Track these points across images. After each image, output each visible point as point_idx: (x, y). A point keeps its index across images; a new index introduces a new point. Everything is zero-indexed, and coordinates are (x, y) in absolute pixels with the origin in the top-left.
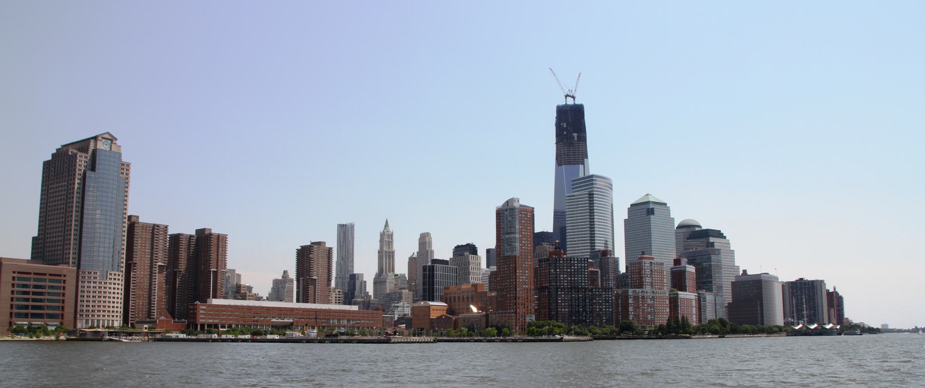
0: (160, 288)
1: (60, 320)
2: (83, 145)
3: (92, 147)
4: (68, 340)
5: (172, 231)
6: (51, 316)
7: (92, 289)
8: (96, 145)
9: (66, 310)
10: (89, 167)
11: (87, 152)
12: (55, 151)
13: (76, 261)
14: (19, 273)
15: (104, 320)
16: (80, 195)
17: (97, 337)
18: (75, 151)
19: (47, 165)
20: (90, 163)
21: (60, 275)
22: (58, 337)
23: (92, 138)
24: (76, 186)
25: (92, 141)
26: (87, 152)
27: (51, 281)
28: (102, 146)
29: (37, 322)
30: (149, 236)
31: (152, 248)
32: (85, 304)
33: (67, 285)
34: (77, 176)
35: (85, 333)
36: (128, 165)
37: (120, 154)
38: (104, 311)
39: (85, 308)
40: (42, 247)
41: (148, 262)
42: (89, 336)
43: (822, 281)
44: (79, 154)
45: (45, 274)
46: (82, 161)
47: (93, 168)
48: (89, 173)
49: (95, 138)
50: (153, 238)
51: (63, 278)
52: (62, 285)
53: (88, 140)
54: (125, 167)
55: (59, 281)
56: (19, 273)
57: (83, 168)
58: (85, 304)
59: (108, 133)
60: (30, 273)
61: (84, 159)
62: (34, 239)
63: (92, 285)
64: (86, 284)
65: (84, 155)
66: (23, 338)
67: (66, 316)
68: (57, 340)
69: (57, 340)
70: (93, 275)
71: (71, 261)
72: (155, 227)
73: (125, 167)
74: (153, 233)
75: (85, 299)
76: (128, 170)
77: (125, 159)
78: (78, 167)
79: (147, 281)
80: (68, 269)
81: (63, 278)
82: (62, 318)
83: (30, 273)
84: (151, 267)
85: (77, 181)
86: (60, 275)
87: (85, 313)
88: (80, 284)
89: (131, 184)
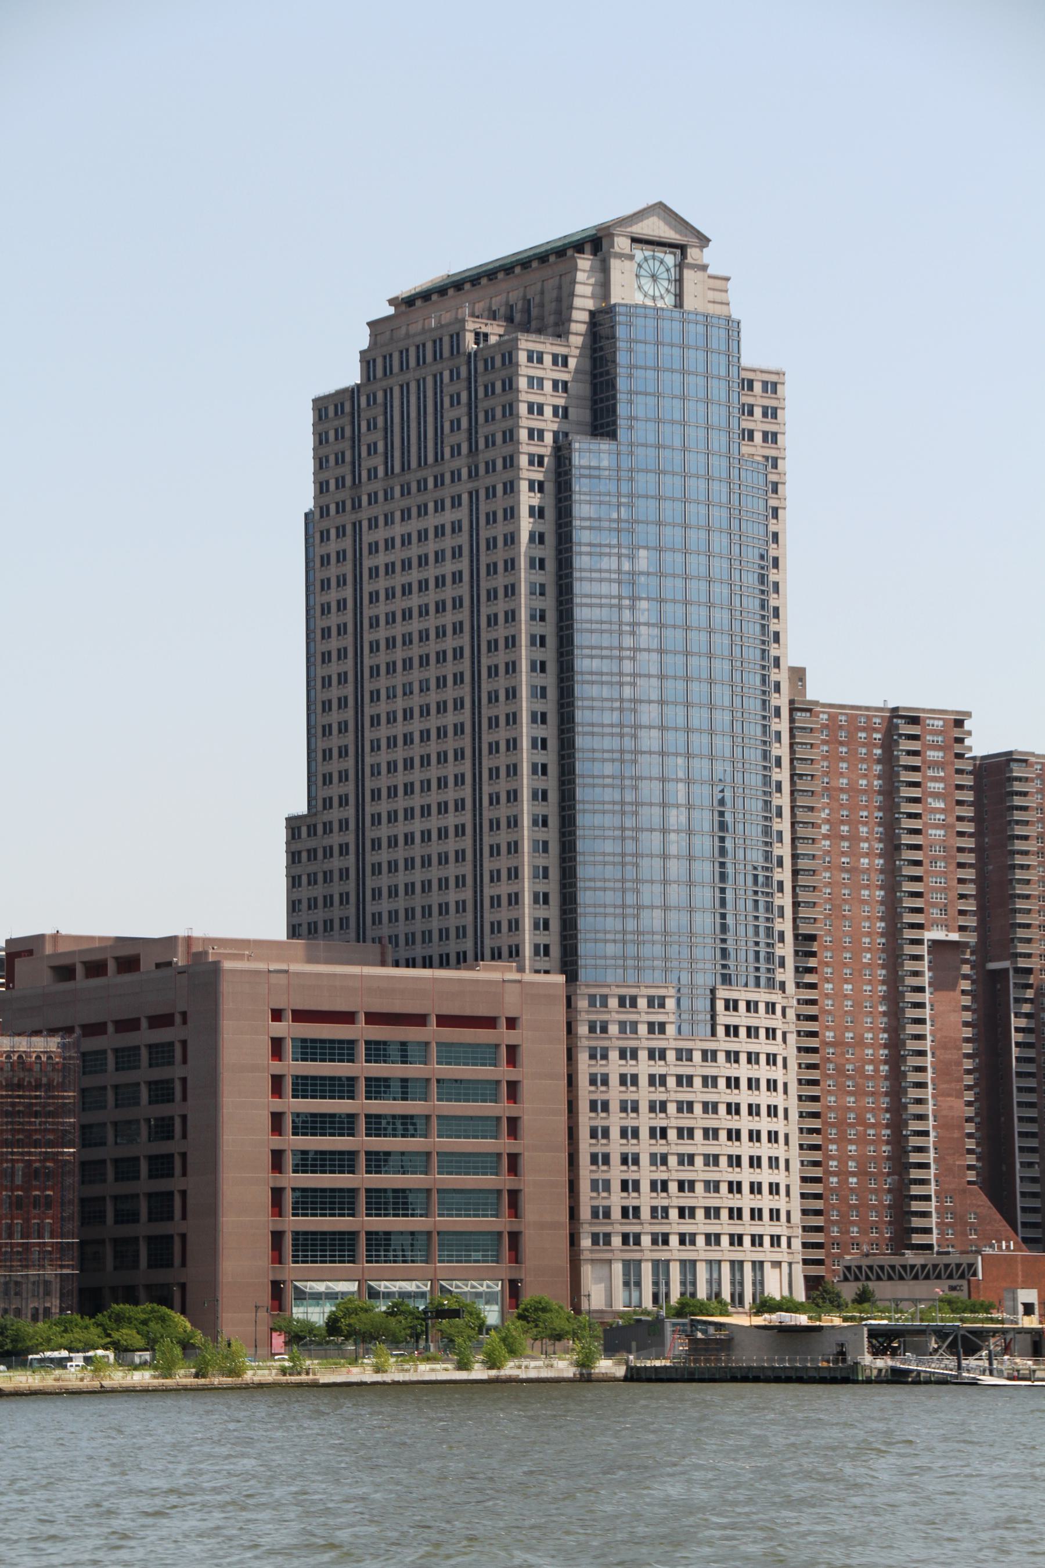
0: (943, 1071)
1: (505, 1269)
2: (532, 284)
3: (584, 300)
4: (634, 1376)
5: (982, 743)
6: (460, 1245)
7: (644, 1094)
8: (604, 286)
9: (530, 1210)
10: (580, 414)
11: (560, 330)
12: (363, 340)
13: (552, 938)
14: (300, 1016)
15: (688, 1266)
16: (548, 577)
17: (713, 1363)
18: (495, 331)
19: (337, 419)
20: (581, 389)
21: (489, 1022)
22: (585, 1363)
23: (578, 246)
24: (526, 525)
25: (584, 263)
26: (560, 330)
27: (450, 1053)
28: (634, 284)
29: (403, 1283)
30: (869, 778)
31: (892, 848)
32: (616, 1173)
33: (526, 1073)
34: (528, 473)
35: (726, 1341)
36: (772, 387)
37: (732, 328)
38: (713, 1213)
39: (616, 1200)
40: (335, 869)
41: (872, 926)
42: (748, 1357)
43: (315, 401)
44: (526, 343)
45: (420, 1020)
46: (543, 376)
47: (602, 421)
48: (589, 455)
49: (596, 243)
50: (890, 792)
51: (504, 1036)
52: (503, 1072)
53: (557, 256)
54: (757, 400)
55: (486, 1054)
56: (300, 1016)
57: (549, 423)
58: (616, 1173)
59: (661, 209)
60: (347, 1018)
61: (549, 372)
62: (294, 825)
63: (644, 1067)
64: (615, 1066)
65: (548, 347)
66: (425, 1371)
67: (529, 1244)
68: (586, 1378)
69: (586, 1378)
70: (644, 1015)
71: (528, 938)
72: (898, 726)
73: (758, 398)
74: (889, 760)
75: (616, 1146)
76: (771, 413)
77: (754, 355)
78: (526, 421)
79: (873, 1031)
80: (515, 983)
81: (504, 1036)
82: (516, 1255)
83: (347, 1018)
84: (894, 956)
85: (527, 499)
86: (489, 1022)
87: (618, 1227)
88: (584, 1066)
89: (790, 490)
